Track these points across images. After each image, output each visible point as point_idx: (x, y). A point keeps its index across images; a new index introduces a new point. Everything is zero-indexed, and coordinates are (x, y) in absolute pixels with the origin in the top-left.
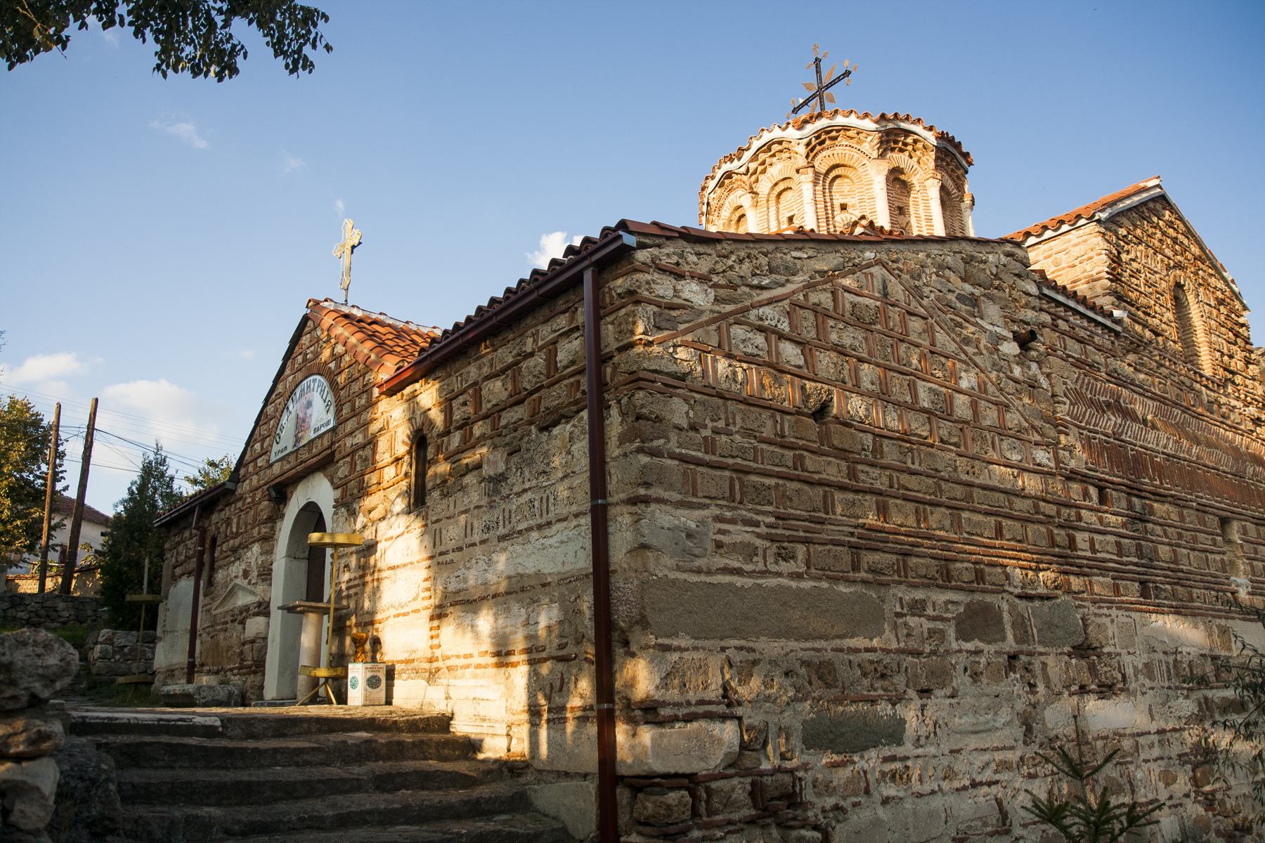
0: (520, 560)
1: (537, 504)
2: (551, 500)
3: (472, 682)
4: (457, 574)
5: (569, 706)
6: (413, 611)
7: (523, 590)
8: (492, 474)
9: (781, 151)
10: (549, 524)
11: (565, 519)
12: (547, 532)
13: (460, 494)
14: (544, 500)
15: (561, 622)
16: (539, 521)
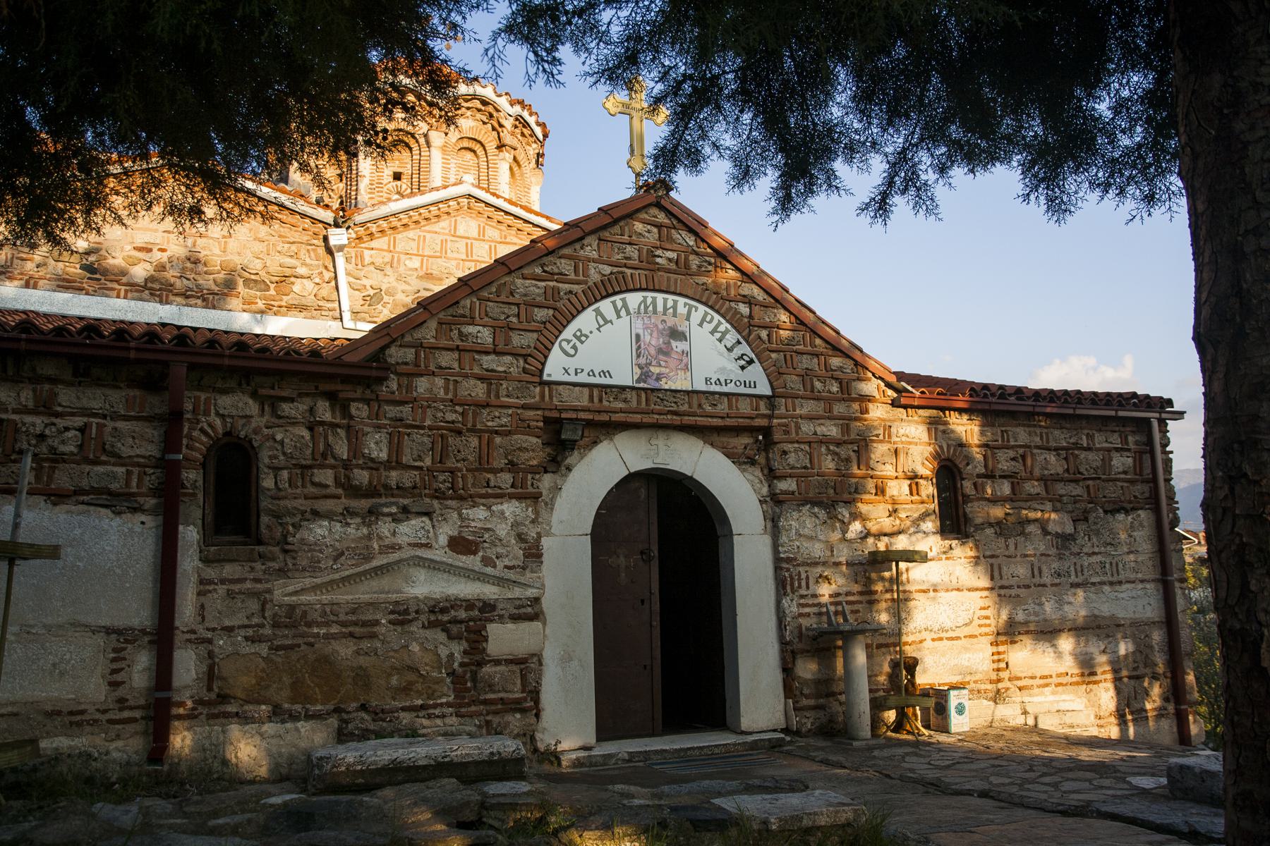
0: (1095, 605)
1: (1107, 566)
2: (1121, 565)
3: (1051, 698)
4: (1026, 607)
5: (299, 724)
6: (965, 637)
7: (1099, 627)
8: (1059, 531)
9: (479, 110)
10: (1120, 583)
11: (1133, 582)
12: (1117, 588)
13: (1021, 539)
14: (1114, 565)
15: (1133, 653)
16: (1111, 579)
